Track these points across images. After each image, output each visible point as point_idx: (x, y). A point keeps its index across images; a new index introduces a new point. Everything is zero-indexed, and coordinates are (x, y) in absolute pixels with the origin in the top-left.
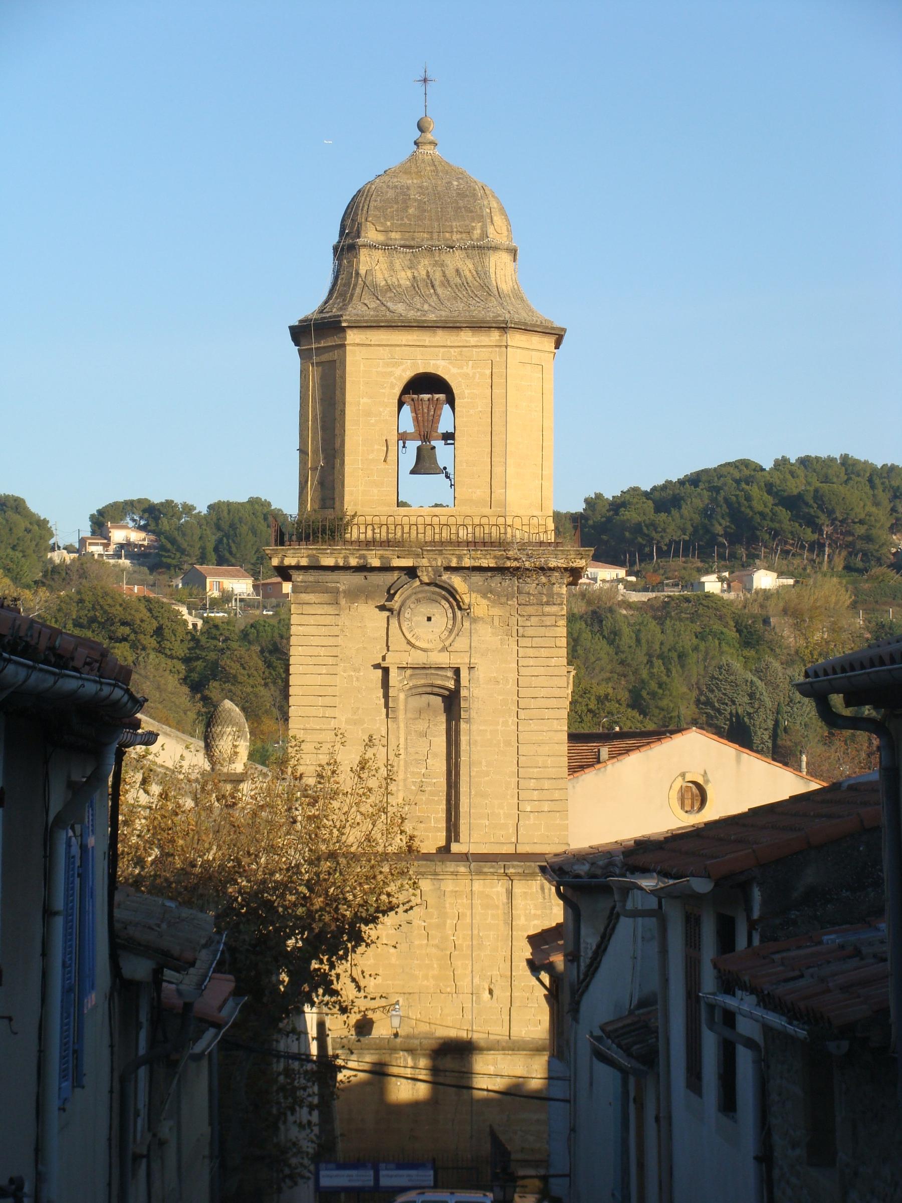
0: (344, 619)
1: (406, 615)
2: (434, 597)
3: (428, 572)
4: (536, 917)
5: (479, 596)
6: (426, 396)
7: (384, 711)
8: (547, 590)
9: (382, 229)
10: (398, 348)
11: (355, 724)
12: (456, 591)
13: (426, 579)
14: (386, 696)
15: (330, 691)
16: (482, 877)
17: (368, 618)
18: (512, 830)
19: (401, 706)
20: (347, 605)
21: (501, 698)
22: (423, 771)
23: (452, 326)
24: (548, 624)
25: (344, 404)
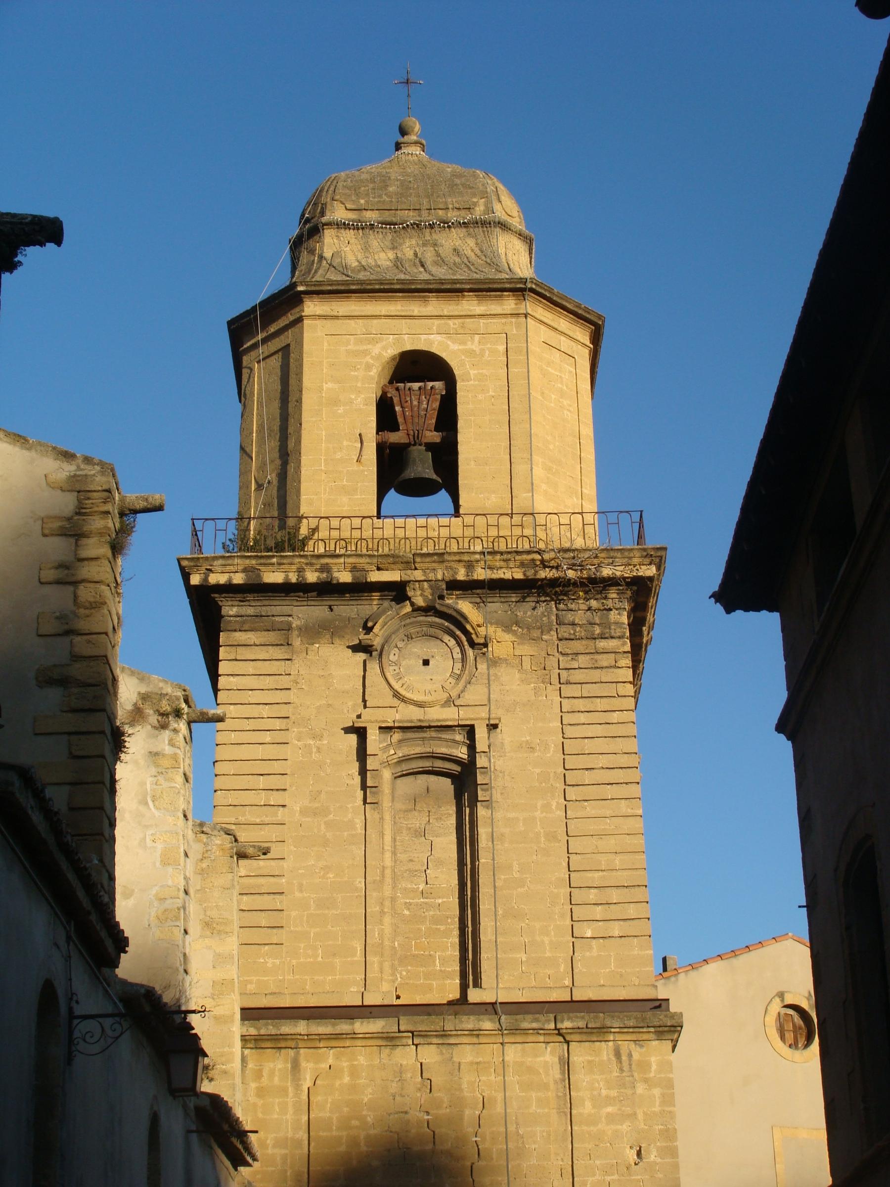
0: (296, 667)
1: (392, 657)
2: (432, 631)
3: (422, 589)
4: (609, 1101)
5: (499, 630)
6: (416, 386)
7: (360, 794)
8: (601, 618)
9: (353, 207)
10: (375, 321)
11: (315, 814)
12: (466, 618)
13: (420, 602)
14: (363, 772)
15: (277, 767)
16: (519, 1039)
17: (337, 663)
18: (564, 967)
19: (386, 788)
20: (303, 647)
21: (538, 771)
22: (422, 886)
23: (450, 290)
24: (605, 664)
25: (301, 391)
